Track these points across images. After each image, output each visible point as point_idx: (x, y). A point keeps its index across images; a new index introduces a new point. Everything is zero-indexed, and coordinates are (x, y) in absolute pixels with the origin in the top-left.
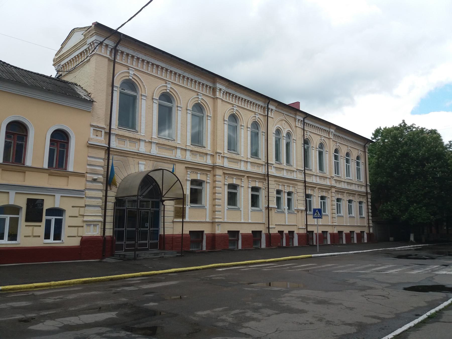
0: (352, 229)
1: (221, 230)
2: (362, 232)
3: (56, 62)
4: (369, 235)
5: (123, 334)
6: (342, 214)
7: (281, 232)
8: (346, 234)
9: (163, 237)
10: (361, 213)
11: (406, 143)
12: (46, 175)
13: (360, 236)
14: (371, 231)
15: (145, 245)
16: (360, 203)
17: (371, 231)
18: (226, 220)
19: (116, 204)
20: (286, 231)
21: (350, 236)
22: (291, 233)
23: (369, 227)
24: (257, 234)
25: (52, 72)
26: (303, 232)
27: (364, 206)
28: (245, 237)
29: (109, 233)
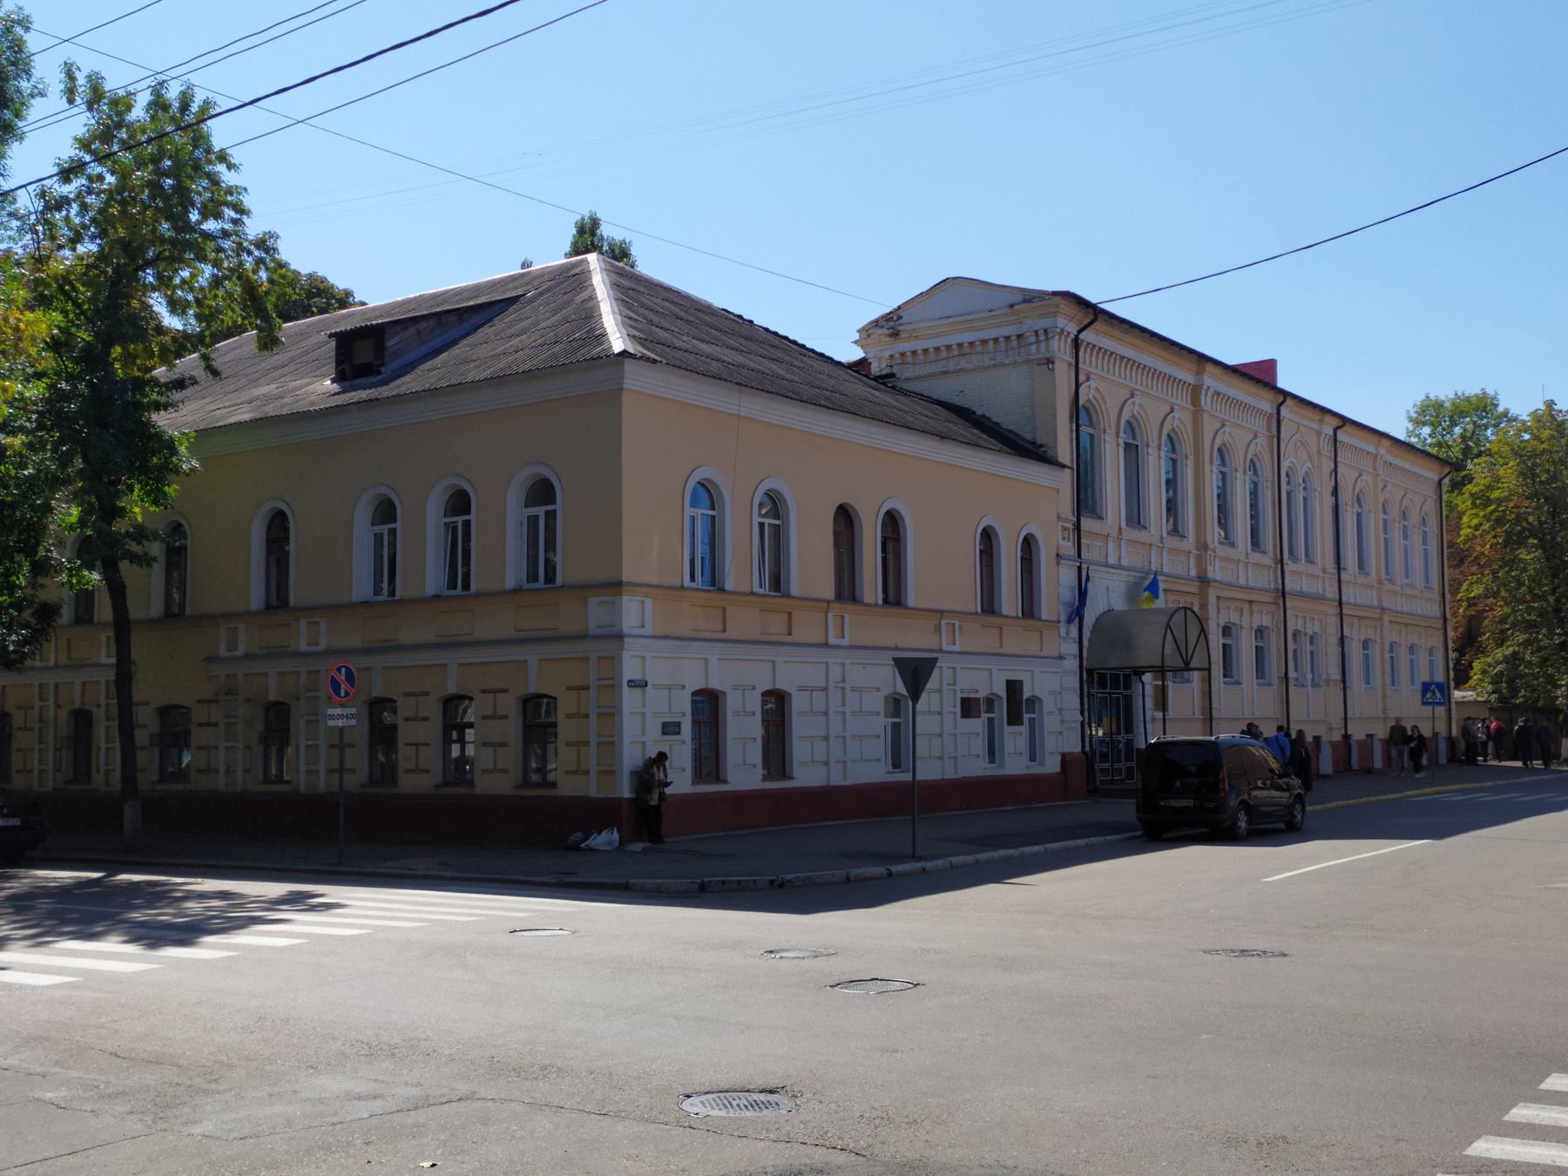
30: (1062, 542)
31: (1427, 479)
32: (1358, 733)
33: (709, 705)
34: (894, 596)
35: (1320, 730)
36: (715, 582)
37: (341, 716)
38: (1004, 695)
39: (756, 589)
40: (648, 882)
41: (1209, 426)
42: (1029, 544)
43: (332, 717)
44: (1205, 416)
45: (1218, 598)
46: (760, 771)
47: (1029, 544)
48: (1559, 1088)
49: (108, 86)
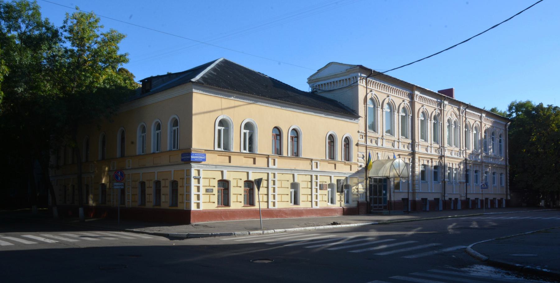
0: (495, 197)
1: (418, 198)
2: (502, 199)
3: (311, 81)
4: (507, 201)
5: (512, 278)
6: (495, 185)
7: (450, 199)
8: (498, 200)
9: (390, 202)
10: (501, 184)
11: (115, 58)
12: (326, 163)
13: (500, 201)
14: (509, 198)
15: (381, 207)
16: (501, 174)
17: (509, 198)
18: (420, 191)
19: (532, 204)
20: (453, 199)
21: (493, 202)
22: (456, 199)
23: (507, 194)
24: (437, 200)
25: (307, 88)
26: (463, 198)
27: (504, 177)
28: (431, 202)
29: (368, 200)
30: (359, 139)
31: (501, 124)
32: (472, 197)
33: (224, 185)
34: (296, 154)
35: (458, 197)
36: (227, 148)
37: (118, 186)
38: (336, 183)
39: (243, 151)
40: (314, 216)
41: (417, 106)
42: (347, 141)
43: (116, 186)
44: (416, 103)
45: (419, 157)
46: (242, 204)
47: (347, 141)
48: (327, 97)
49: (127, 56)
